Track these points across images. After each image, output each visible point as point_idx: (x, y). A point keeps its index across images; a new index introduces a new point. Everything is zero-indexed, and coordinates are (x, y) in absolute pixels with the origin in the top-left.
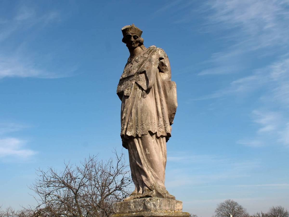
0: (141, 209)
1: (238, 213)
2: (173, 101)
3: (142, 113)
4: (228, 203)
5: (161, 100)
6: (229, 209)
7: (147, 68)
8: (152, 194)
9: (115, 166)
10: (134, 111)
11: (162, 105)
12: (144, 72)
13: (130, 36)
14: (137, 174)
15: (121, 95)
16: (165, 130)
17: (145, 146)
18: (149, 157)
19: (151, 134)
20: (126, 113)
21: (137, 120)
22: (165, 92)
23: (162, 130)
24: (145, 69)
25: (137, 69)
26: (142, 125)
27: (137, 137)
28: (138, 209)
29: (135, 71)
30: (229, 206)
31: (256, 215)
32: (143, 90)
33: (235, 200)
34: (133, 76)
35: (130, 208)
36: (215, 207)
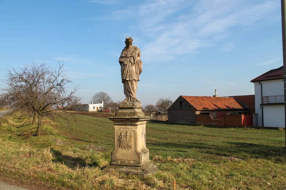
0: (132, 105)
1: (107, 100)
2: (141, 68)
3: (132, 72)
4: (101, 93)
5: (137, 67)
6: (101, 98)
7: (135, 56)
8: (135, 100)
9: (57, 71)
10: (129, 71)
11: (137, 69)
12: (133, 57)
13: (130, 42)
14: (128, 93)
15: (121, 63)
16: (138, 79)
17: (132, 84)
18: (133, 88)
19: (134, 80)
20: (126, 71)
21: (130, 74)
22: (206, 112)
23: (137, 79)
24: (134, 56)
25: (130, 55)
26: (132, 77)
27: (130, 81)
28: (130, 105)
29: (129, 56)
30: (101, 95)
31: (118, 102)
32: (132, 63)
33: (106, 92)
34: (128, 57)
35: (127, 105)
36: (93, 95)
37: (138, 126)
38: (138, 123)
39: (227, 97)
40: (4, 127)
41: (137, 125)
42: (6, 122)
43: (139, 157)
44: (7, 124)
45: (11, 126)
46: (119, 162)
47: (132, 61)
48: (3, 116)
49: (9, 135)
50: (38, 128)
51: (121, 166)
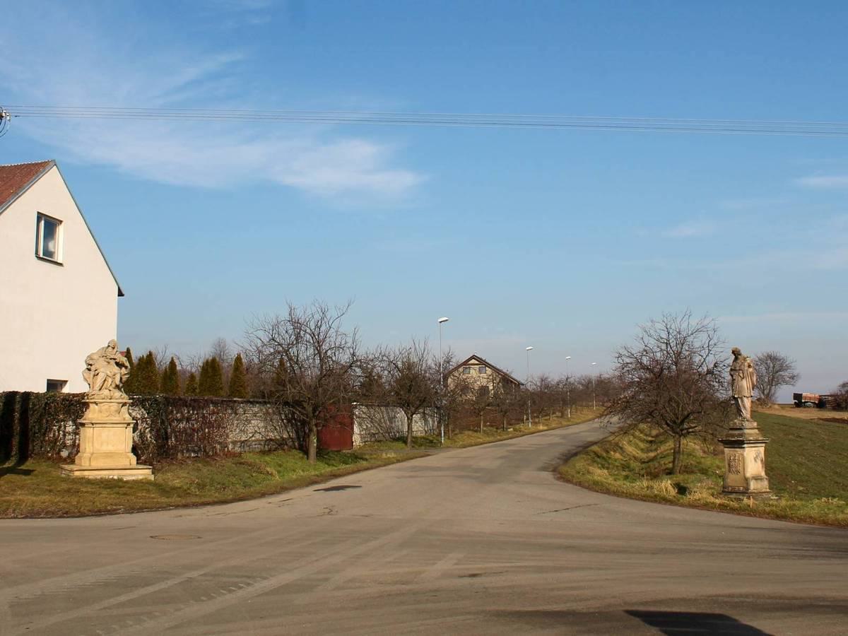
17: (742, 401)
37: (747, 449)
38: (745, 446)
39: (411, 477)
40: (616, 460)
41: (744, 448)
42: (619, 450)
43: (747, 484)
44: (621, 455)
45: (630, 459)
46: (730, 489)
47: (742, 375)
48: (610, 436)
49: (624, 473)
50: (674, 462)
51: (731, 493)
